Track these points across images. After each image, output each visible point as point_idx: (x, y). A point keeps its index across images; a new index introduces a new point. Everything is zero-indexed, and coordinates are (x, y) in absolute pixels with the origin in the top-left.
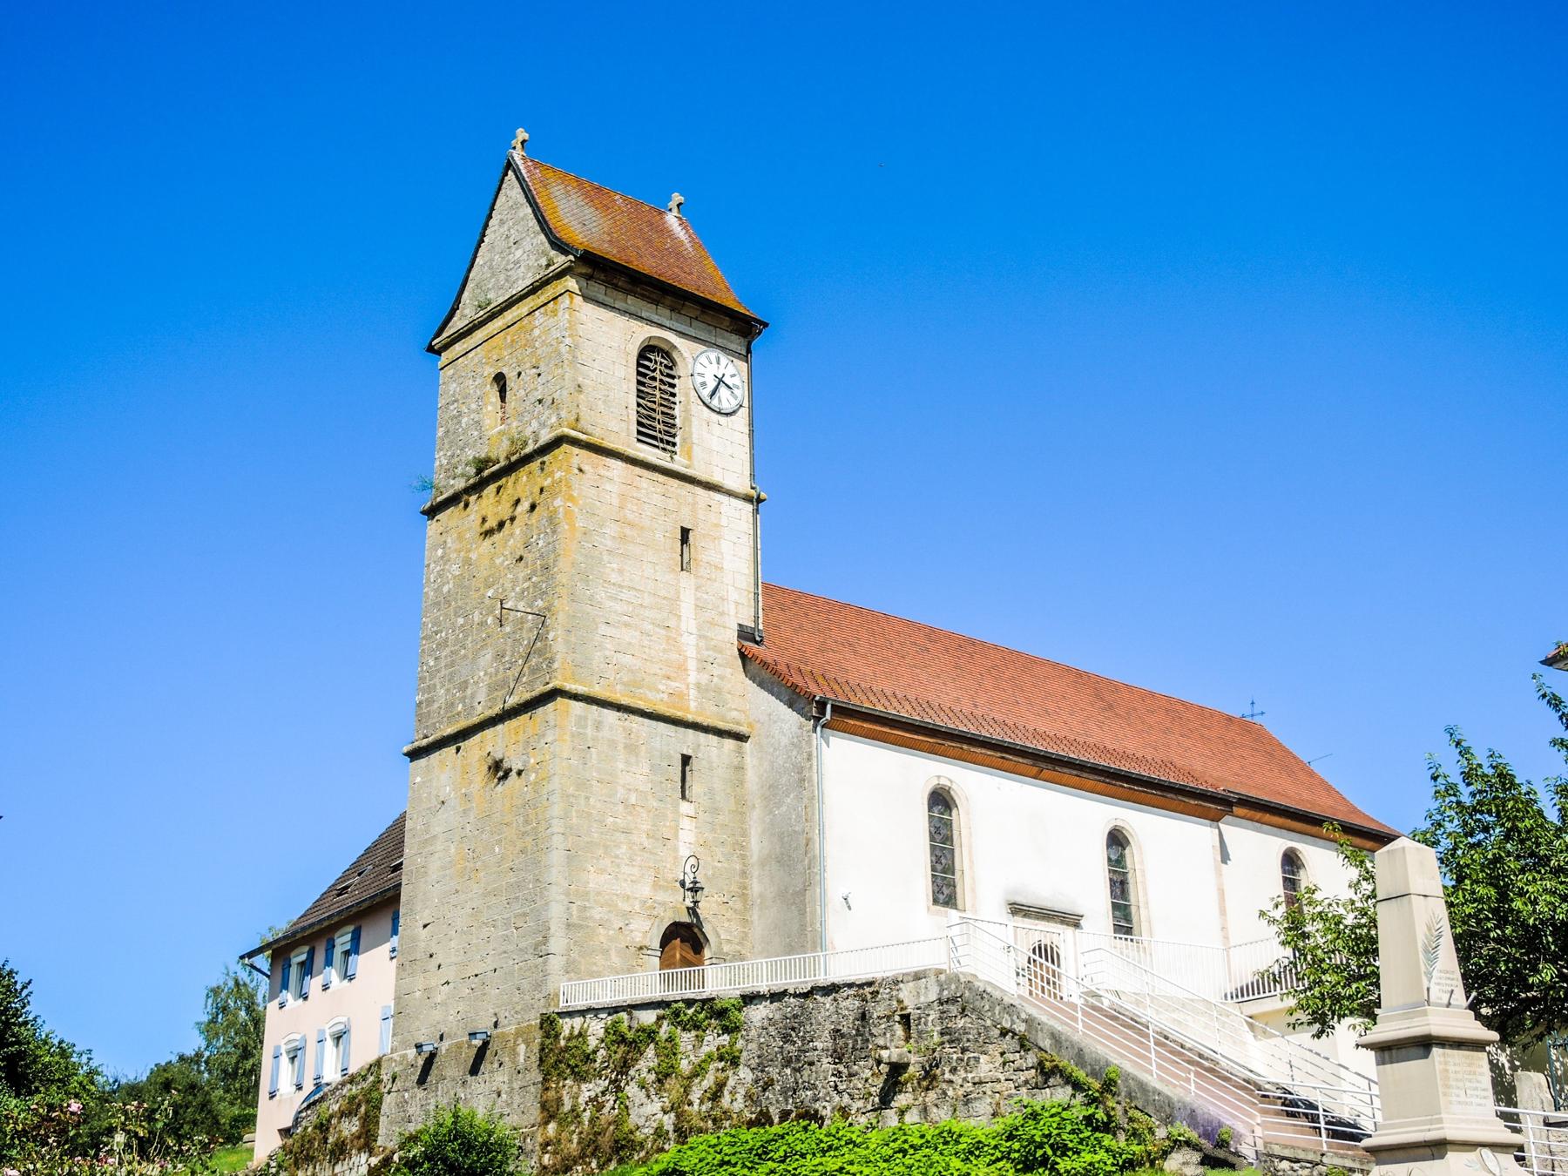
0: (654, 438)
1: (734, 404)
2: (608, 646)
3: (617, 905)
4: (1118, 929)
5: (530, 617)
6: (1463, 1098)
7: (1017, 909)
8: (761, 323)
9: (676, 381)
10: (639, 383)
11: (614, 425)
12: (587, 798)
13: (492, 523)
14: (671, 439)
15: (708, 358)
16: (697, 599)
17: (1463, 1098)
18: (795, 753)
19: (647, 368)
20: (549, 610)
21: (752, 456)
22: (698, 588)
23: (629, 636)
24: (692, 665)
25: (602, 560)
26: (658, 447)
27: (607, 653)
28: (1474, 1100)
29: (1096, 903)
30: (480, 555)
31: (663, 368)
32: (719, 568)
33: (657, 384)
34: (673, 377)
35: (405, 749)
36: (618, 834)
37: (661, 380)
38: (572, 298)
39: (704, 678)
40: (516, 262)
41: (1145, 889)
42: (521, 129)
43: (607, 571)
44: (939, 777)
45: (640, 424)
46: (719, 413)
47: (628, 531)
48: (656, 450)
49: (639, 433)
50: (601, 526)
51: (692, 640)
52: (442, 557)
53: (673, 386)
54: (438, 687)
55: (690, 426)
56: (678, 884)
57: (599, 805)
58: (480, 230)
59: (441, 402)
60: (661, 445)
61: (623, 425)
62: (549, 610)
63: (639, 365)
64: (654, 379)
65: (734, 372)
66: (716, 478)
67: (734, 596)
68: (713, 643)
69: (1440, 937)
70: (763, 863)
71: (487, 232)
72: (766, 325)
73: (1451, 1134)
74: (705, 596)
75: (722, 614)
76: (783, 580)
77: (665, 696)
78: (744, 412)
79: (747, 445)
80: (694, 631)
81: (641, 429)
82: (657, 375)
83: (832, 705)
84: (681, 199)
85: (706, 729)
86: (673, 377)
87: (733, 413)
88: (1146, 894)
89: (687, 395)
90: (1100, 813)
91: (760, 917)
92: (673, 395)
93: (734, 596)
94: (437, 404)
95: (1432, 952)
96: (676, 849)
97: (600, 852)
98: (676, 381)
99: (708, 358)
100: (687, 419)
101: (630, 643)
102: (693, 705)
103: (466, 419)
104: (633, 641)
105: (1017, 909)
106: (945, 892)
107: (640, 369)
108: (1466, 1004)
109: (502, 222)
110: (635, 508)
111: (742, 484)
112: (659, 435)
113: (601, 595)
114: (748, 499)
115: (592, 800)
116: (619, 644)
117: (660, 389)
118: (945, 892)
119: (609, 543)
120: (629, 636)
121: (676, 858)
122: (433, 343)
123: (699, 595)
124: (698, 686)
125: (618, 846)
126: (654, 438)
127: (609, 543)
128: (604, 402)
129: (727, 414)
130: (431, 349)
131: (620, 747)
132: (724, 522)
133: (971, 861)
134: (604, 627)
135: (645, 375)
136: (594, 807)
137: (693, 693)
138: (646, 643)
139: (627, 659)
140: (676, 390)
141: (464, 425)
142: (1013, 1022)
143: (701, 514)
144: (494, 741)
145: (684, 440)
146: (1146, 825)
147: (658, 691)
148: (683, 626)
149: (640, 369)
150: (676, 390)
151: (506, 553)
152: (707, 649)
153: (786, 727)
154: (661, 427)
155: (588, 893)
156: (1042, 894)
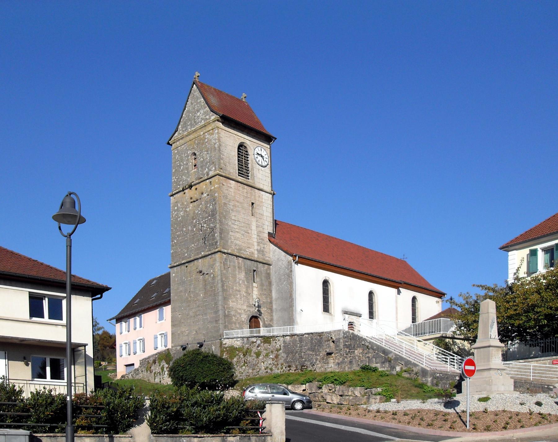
0: (243, 174)
1: (266, 164)
2: (232, 238)
3: (237, 311)
4: (370, 318)
5: (208, 229)
6: (495, 359)
7: (346, 313)
8: (274, 138)
9: (248, 156)
10: (238, 157)
11: (232, 171)
12: (228, 282)
13: (194, 199)
14: (247, 175)
15: (258, 149)
16: (256, 224)
17: (495, 359)
18: (287, 270)
19: (240, 152)
20: (215, 228)
21: (271, 180)
22: (257, 221)
23: (238, 235)
24: (256, 244)
25: (230, 212)
26: (244, 177)
27: (232, 240)
28: (497, 360)
29: (365, 311)
30: (190, 209)
31: (245, 152)
32: (262, 215)
33: (243, 157)
34: (248, 155)
35: (169, 266)
36: (237, 292)
37: (245, 156)
38: (218, 130)
39: (259, 248)
40: (198, 117)
41: (378, 307)
42: (197, 72)
43: (231, 216)
44: (326, 277)
45: (239, 170)
46: (262, 167)
47: (237, 204)
48: (243, 178)
49: (239, 173)
50: (229, 202)
51: (256, 236)
52: (177, 210)
53: (248, 158)
54: (178, 248)
55: (253, 170)
56: (253, 306)
57: (231, 284)
58: (184, 105)
59: (173, 161)
60: (245, 177)
61: (234, 170)
62: (215, 228)
63: (238, 151)
64: (242, 155)
65: (266, 154)
66: (261, 187)
67: (267, 223)
68: (261, 237)
69: (494, 323)
70: (276, 300)
71: (187, 106)
72: (276, 139)
73: (492, 367)
74: (259, 224)
75: (263, 229)
76: (284, 218)
77: (248, 253)
78: (269, 166)
79: (270, 177)
80: (256, 234)
81: (240, 172)
82: (243, 154)
83: (298, 257)
84: (245, 95)
85: (260, 262)
86: (248, 155)
87: (266, 167)
88: (378, 309)
89: (252, 161)
90: (411, 294)
91: (275, 314)
92: (248, 160)
93: (267, 223)
94: (172, 161)
95: (492, 325)
96: (252, 296)
97: (233, 297)
98: (248, 156)
99: (258, 149)
100: (253, 169)
101: (238, 237)
102: (256, 256)
103: (182, 167)
104: (239, 237)
105: (346, 313)
106: (326, 309)
107: (239, 153)
108: (498, 338)
109: (192, 104)
110: (239, 196)
111: (269, 189)
112: (244, 173)
113: (230, 223)
114: (271, 194)
115: (230, 282)
116: (235, 238)
117: (244, 159)
118: (326, 309)
119: (232, 207)
120: (238, 235)
121: (252, 298)
122: (170, 142)
123: (257, 223)
124: (257, 250)
125: (237, 295)
126: (243, 174)
127: (232, 207)
128: (229, 163)
129: (264, 167)
130: (168, 144)
131: (237, 268)
132: (264, 201)
133: (333, 300)
134: (231, 232)
135: (240, 154)
136: (230, 284)
137: (256, 252)
138: (242, 237)
139: (238, 242)
140: (249, 159)
141: (182, 169)
142: (365, 343)
143: (257, 198)
144: (187, 265)
145: (251, 175)
146: (379, 289)
147: (246, 252)
148: (253, 233)
149: (239, 153)
150: (249, 159)
151: (199, 209)
152: (260, 239)
153: (284, 262)
154: (245, 171)
155: (230, 307)
156: (352, 308)
